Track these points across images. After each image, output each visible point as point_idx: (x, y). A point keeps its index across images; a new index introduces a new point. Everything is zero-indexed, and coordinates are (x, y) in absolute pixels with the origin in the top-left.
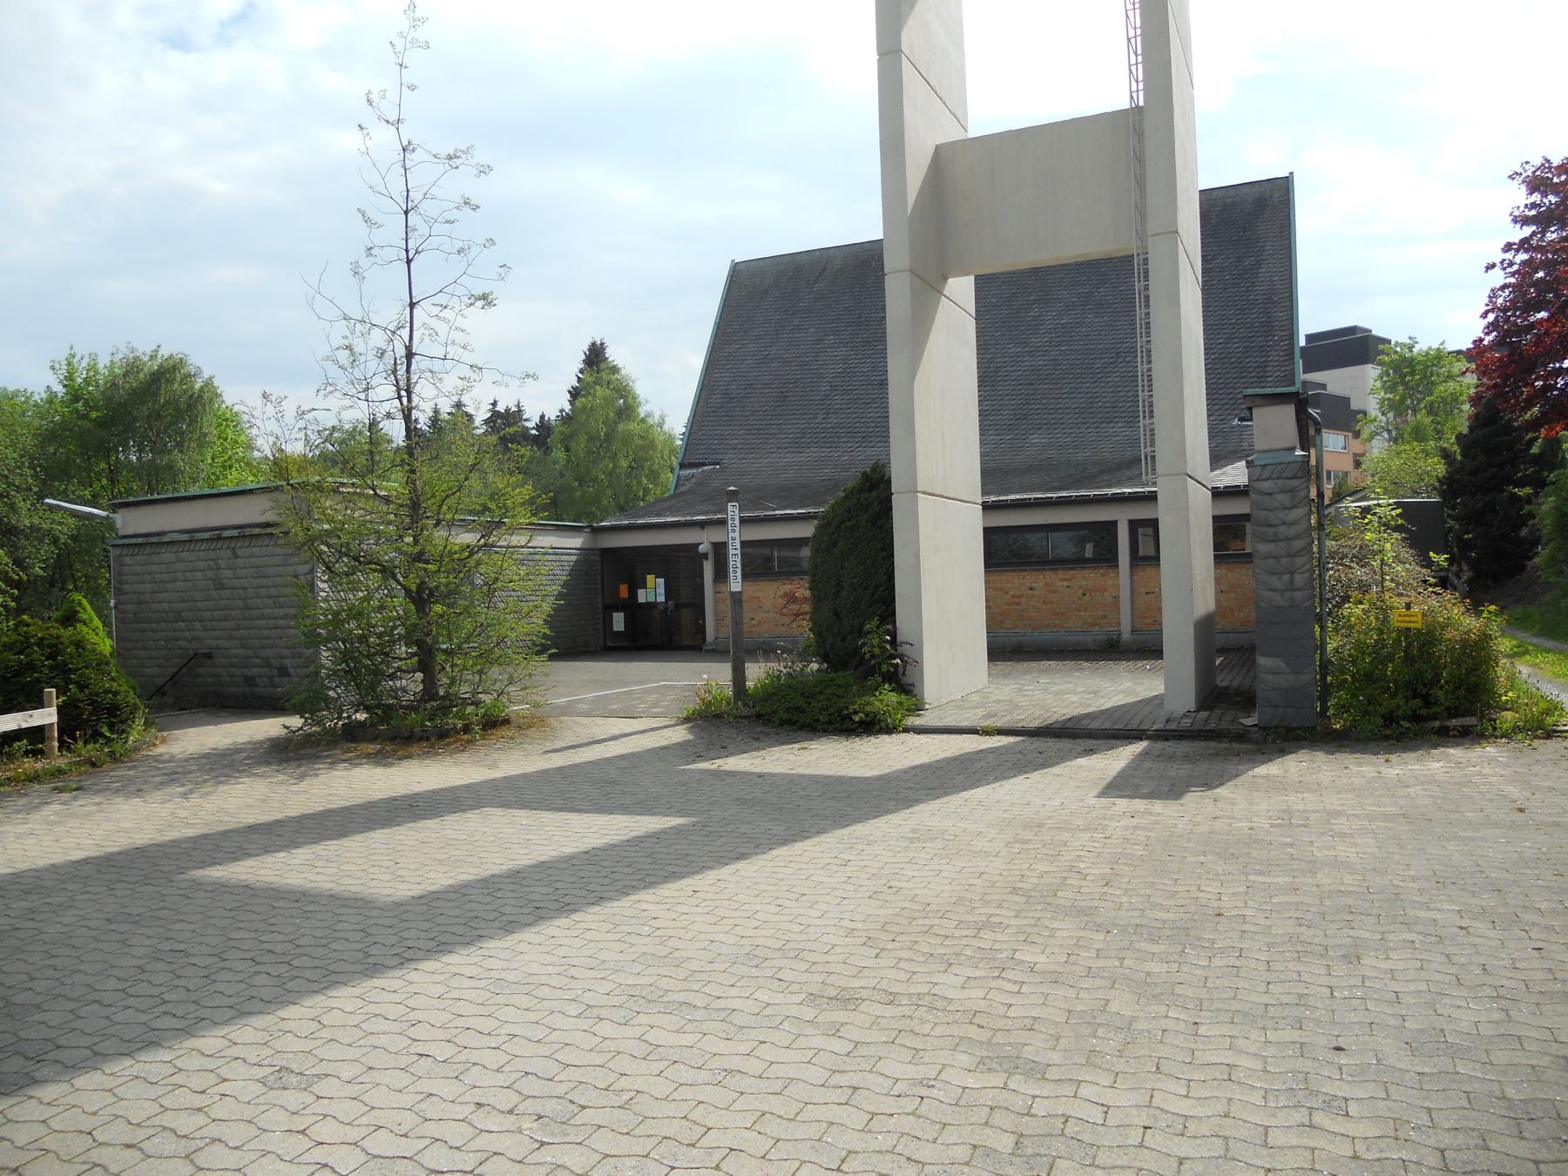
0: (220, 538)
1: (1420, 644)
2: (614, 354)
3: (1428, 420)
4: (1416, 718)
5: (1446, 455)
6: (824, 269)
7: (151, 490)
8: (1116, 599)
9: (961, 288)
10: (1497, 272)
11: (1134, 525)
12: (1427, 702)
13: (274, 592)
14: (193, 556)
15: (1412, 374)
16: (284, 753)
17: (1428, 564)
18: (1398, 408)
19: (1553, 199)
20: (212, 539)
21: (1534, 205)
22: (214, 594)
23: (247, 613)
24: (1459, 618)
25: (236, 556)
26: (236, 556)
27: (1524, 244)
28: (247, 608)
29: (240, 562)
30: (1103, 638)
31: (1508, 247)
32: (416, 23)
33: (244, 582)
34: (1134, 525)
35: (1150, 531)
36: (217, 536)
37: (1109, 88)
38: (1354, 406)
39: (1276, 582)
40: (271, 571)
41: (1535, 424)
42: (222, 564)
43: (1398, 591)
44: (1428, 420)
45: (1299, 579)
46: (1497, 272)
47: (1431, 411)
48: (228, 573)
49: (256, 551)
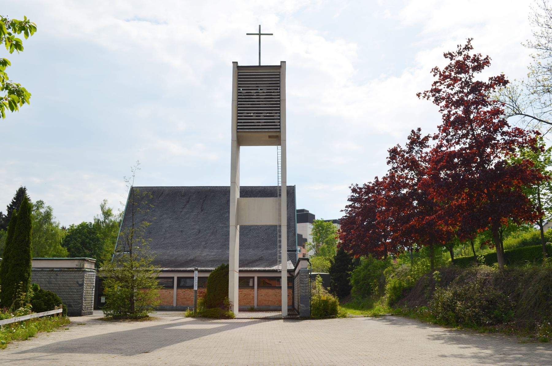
0: (53, 270)
1: (326, 302)
2: (33, 197)
3: (326, 246)
4: (325, 315)
5: (331, 261)
6: (162, 193)
7: (38, 256)
8: (253, 297)
9: (238, 226)
10: (344, 212)
11: (179, 278)
12: (327, 312)
13: (69, 285)
14: (41, 275)
15: (322, 228)
16: (106, 320)
17: (326, 289)
18: (316, 240)
19: (357, 195)
20: (49, 271)
21: (353, 196)
22: (48, 285)
23: (59, 291)
24: (332, 298)
25: (57, 275)
26: (57, 275)
27: (350, 206)
28: (60, 289)
29: (58, 277)
30: (250, 307)
31: (347, 207)
32: (139, 164)
33: (60, 282)
34: (179, 278)
35: (172, 280)
36: (52, 270)
37: (243, 149)
38: (304, 237)
39: (303, 291)
40: (69, 280)
41: (352, 255)
42: (52, 277)
43: (321, 293)
44: (326, 246)
45: (307, 291)
46: (344, 212)
47: (327, 243)
48: (54, 280)
49: (65, 275)
